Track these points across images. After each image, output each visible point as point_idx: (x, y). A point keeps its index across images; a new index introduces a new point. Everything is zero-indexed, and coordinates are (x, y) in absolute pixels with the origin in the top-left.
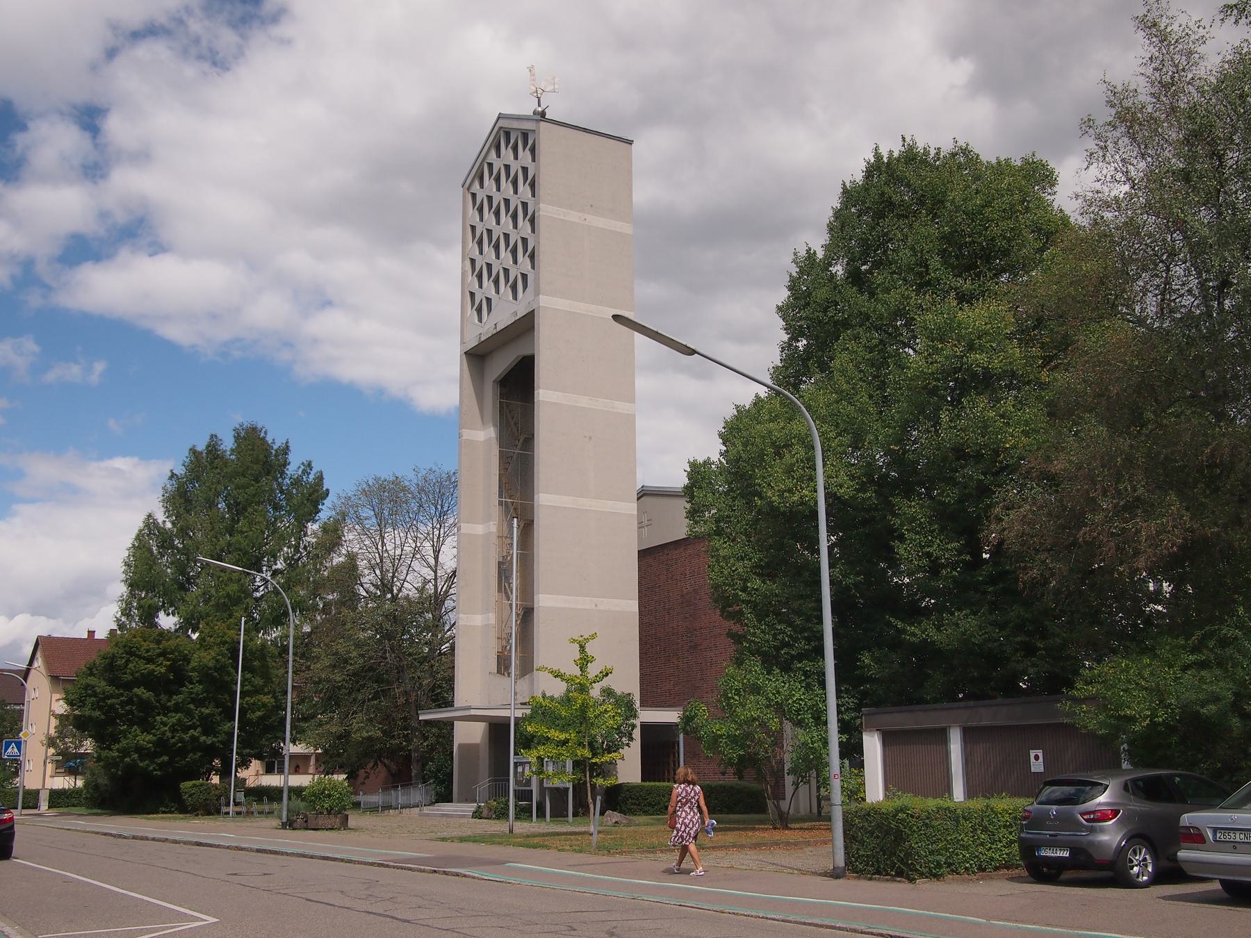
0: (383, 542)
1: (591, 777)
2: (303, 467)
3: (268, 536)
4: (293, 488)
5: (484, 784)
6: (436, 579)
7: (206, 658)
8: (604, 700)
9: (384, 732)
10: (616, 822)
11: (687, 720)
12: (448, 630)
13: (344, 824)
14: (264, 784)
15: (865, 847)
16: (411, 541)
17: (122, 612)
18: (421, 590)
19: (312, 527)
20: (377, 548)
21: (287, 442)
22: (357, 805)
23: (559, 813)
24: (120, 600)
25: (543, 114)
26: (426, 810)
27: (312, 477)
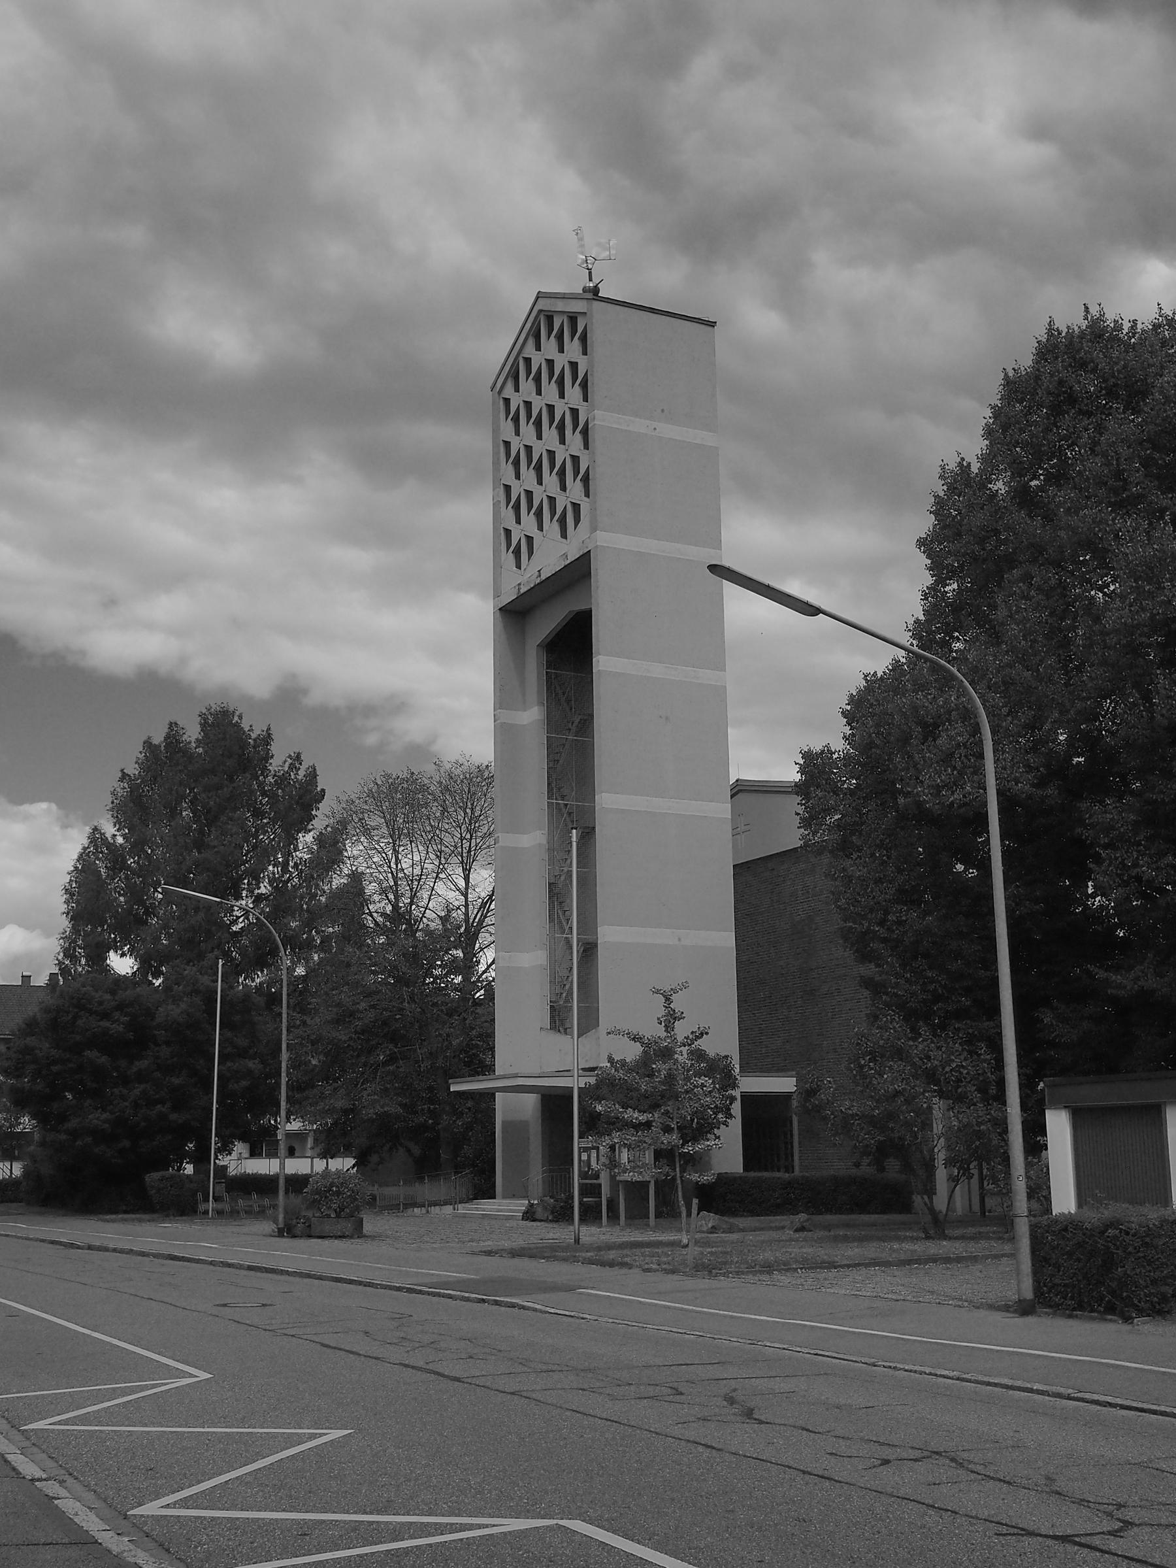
0: (397, 858)
1: (683, 1171)
2: (290, 761)
3: (248, 852)
4: (278, 789)
5: (536, 1174)
6: (466, 906)
7: (173, 1012)
8: (692, 1064)
9: (403, 1106)
10: (713, 1227)
11: (808, 1092)
12: (484, 972)
13: (358, 1232)
14: (249, 1171)
15: (1061, 1273)
16: (432, 856)
17: (64, 953)
18: (444, 920)
19: (306, 839)
20: (390, 867)
21: (269, 729)
22: (372, 1201)
23: (637, 1215)
24: (62, 938)
25: (595, 291)
26: (462, 1209)
27: (302, 773)
